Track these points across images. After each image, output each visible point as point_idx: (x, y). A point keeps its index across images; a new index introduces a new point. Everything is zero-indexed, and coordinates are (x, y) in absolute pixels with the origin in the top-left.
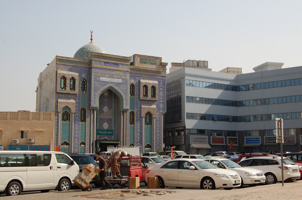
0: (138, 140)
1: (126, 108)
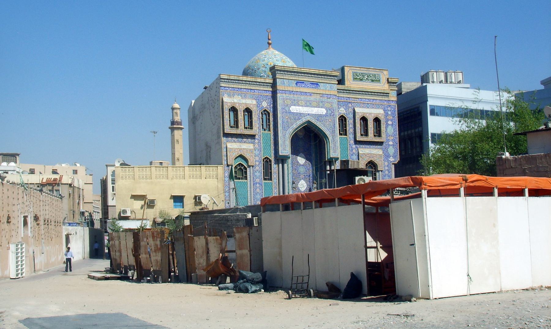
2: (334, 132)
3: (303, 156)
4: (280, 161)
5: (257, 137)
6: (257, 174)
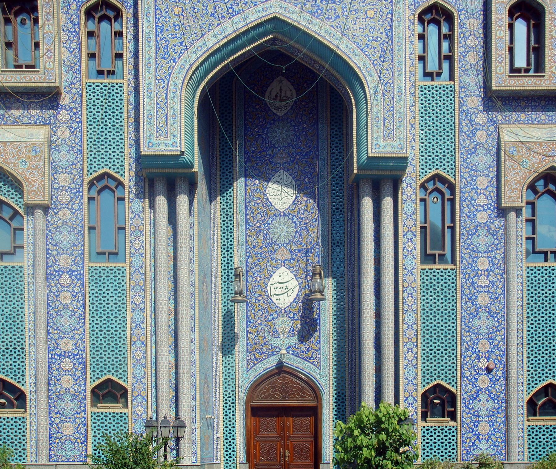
0: (478, 358)
1: (389, 149)
2: (386, 55)
3: (289, 178)
4: (160, 186)
5: (65, 100)
6: (65, 237)
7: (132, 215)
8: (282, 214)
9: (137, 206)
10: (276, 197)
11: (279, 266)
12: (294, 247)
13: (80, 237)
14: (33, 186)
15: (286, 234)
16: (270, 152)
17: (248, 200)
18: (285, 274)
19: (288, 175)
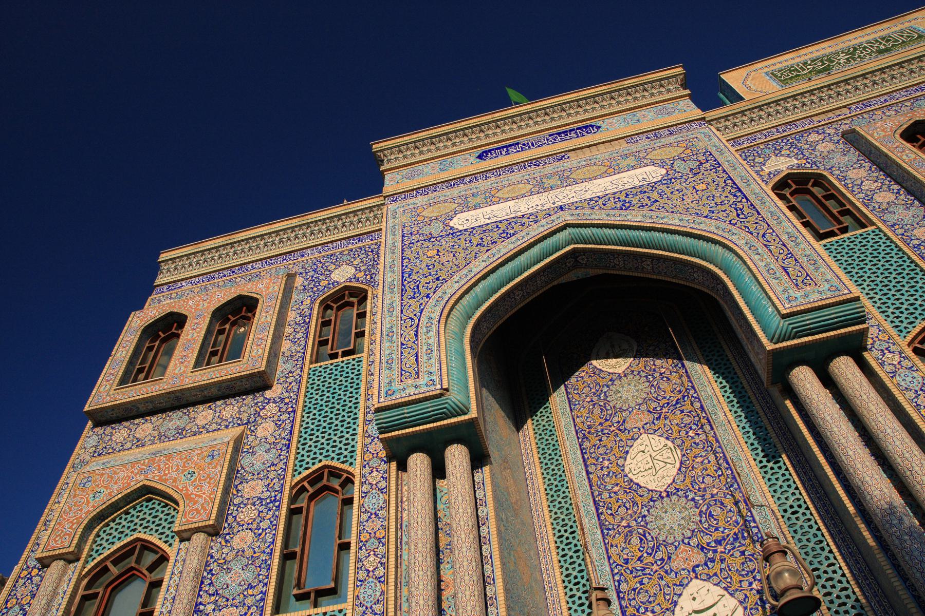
7: (365, 517)
8: (664, 494)
9: (374, 501)
10: (645, 473)
11: (685, 581)
12: (707, 539)
13: (264, 572)
14: (195, 503)
15: (683, 522)
16: (616, 419)
17: (596, 493)
18: (704, 591)
19: (657, 438)
